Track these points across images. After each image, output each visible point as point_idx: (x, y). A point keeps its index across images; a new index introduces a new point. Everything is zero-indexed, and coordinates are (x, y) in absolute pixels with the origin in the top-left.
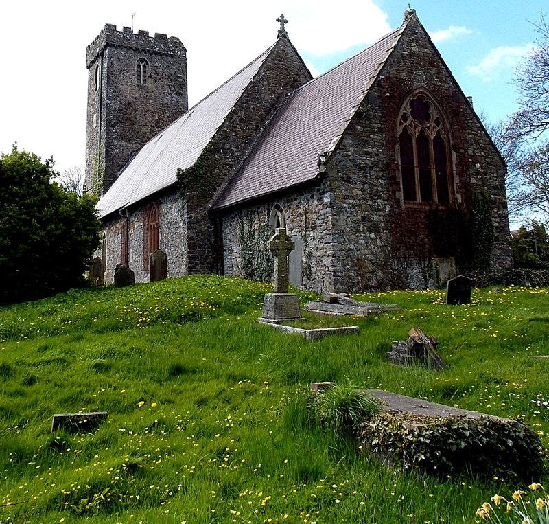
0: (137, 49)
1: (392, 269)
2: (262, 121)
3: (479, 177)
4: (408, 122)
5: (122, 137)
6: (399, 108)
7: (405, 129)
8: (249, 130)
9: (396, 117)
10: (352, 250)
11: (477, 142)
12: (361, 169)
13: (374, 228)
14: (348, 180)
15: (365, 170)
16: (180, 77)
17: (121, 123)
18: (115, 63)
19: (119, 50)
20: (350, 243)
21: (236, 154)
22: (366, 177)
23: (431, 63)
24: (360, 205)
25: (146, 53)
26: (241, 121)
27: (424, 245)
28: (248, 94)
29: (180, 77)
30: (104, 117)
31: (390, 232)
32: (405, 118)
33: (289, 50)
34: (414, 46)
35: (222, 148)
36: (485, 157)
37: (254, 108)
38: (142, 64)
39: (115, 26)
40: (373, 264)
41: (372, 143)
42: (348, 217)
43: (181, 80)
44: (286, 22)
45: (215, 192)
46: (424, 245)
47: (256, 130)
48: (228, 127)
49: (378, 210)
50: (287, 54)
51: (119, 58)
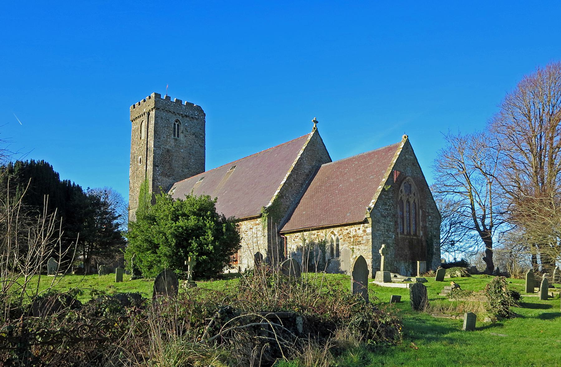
0: (174, 113)
2: (304, 181)
3: (430, 223)
8: (298, 186)
9: (399, 191)
11: (430, 206)
15: (385, 217)
16: (201, 135)
21: (291, 200)
22: (385, 221)
23: (413, 164)
24: (382, 234)
25: (179, 116)
27: (407, 255)
31: (394, 248)
33: (318, 139)
35: (285, 196)
36: (433, 213)
37: (300, 173)
38: (177, 124)
42: (378, 240)
46: (407, 255)
47: (301, 186)
51: (162, 118)
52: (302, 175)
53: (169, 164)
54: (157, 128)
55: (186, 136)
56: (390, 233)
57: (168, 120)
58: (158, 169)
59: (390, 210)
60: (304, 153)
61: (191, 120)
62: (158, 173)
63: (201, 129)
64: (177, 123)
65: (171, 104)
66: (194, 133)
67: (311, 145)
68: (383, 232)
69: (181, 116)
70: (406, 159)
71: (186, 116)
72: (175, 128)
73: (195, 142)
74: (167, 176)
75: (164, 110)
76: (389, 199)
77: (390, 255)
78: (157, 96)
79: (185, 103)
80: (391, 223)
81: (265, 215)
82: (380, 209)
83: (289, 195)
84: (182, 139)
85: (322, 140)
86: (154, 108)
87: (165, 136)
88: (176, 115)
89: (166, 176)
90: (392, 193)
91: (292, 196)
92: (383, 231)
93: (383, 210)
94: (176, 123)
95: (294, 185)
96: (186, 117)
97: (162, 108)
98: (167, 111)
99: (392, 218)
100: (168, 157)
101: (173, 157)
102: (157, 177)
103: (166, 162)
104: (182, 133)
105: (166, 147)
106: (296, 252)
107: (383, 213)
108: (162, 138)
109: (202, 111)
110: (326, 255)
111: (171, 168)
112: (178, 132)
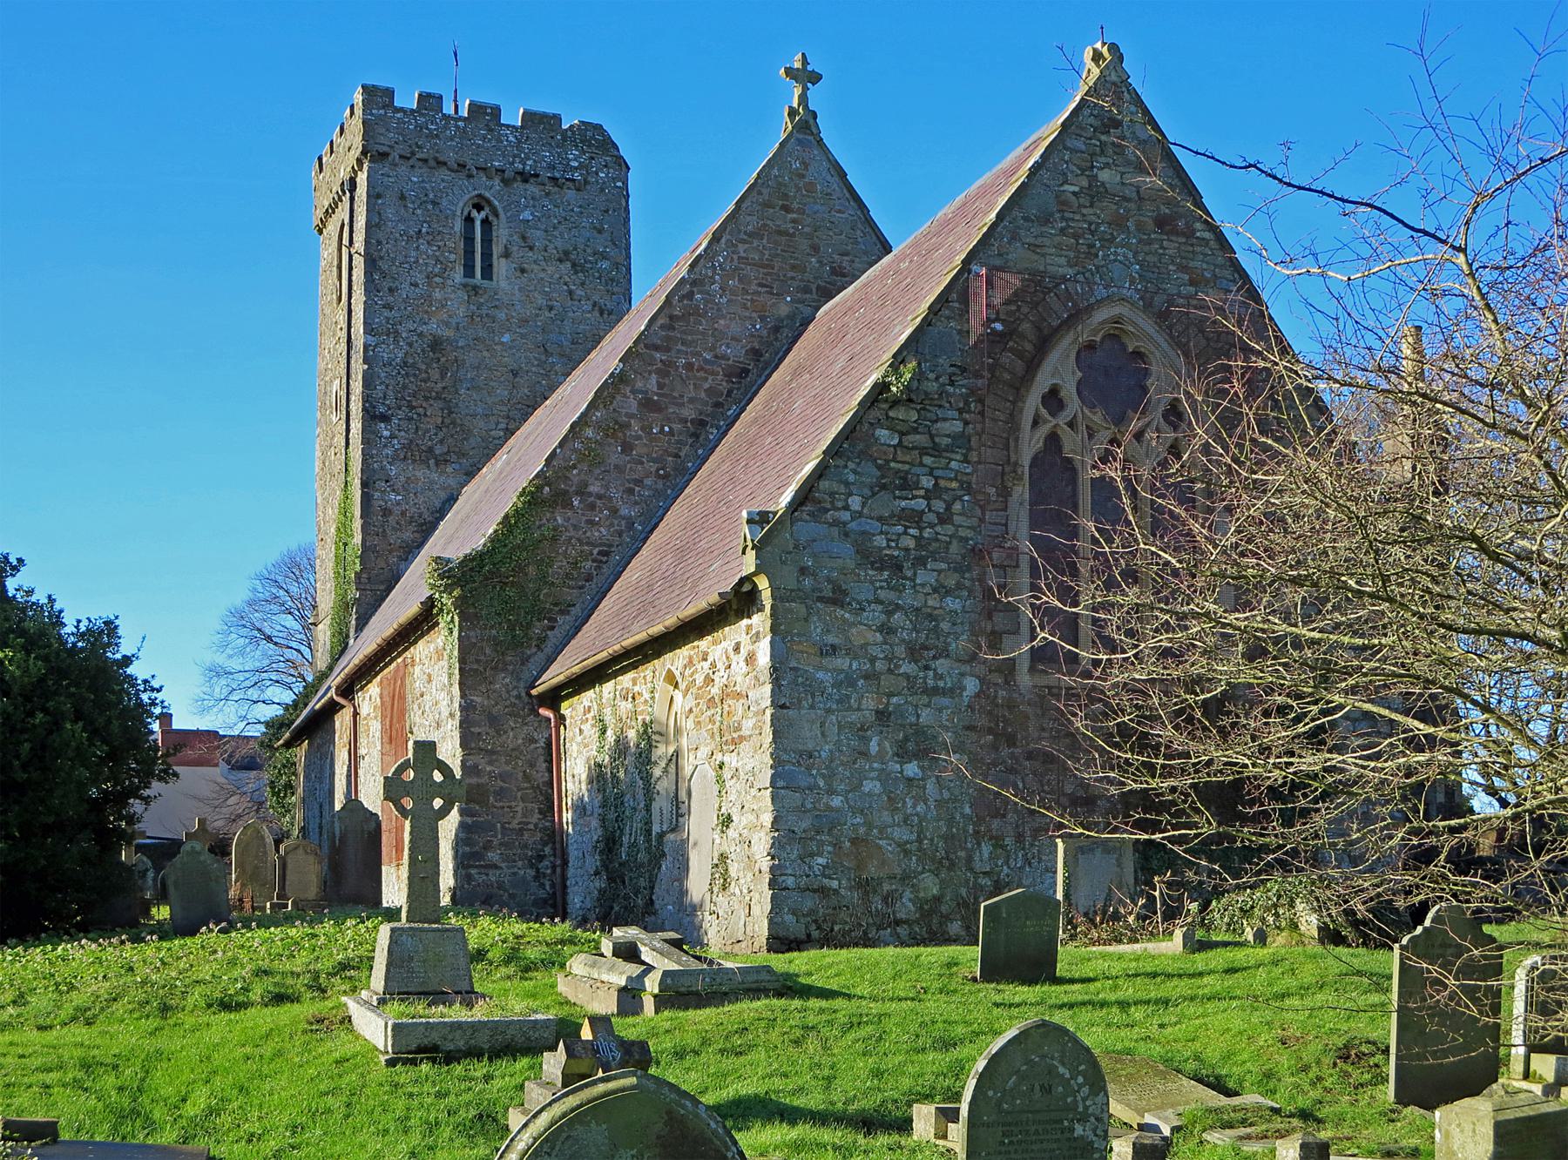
1: (971, 869)
2: (718, 405)
4: (1066, 415)
5: (413, 453)
6: (1033, 365)
7: (1053, 439)
8: (671, 432)
10: (837, 810)
12: (881, 563)
13: (918, 746)
14: (838, 598)
15: (900, 568)
16: (604, 256)
17: (412, 408)
18: (390, 213)
19: (403, 169)
20: (831, 792)
21: (624, 511)
22: (899, 590)
25: (490, 178)
26: (648, 404)
28: (671, 317)
29: (604, 256)
30: (357, 387)
32: (1053, 399)
34: (1107, 165)
35: (580, 493)
37: (689, 366)
38: (478, 217)
39: (390, 93)
40: (907, 853)
41: (927, 482)
42: (829, 711)
43: (605, 265)
44: (815, 78)
45: (552, 628)
47: (696, 436)
48: (598, 426)
49: (936, 691)
50: (810, 187)
51: (403, 197)
52: (702, 374)
53: (440, 404)
54: (379, 243)
55: (523, 271)
56: (942, 665)
57: (434, 203)
58: (386, 433)
59: (944, 519)
60: (716, 254)
61: (548, 194)
62: (389, 452)
63: (600, 232)
64: (483, 214)
65: (446, 127)
66: (566, 253)
67: (767, 205)
68: (873, 660)
69: (497, 181)
70: (1096, 192)
71: (525, 177)
72: (469, 240)
73: (571, 293)
74: (432, 462)
75: (411, 162)
76: (936, 450)
77: (940, 803)
78: (378, 97)
79: (513, 116)
80: (952, 603)
81: (447, 600)
82: (846, 516)
83: (607, 487)
84: (503, 284)
85: (842, 175)
86: (364, 153)
87: (420, 278)
88: (470, 176)
89: (425, 462)
90: (960, 411)
91: (631, 491)
92: (875, 651)
93: (880, 519)
94: (474, 213)
95: (647, 429)
96: (526, 181)
97: (401, 149)
98: (425, 161)
99: (959, 569)
100: (435, 374)
101: (461, 373)
102: (382, 468)
103: (426, 398)
104: (507, 254)
105: (424, 328)
106: (586, 799)
107: (880, 541)
108: (405, 290)
109: (608, 145)
110: (655, 806)
111: (453, 423)
112: (487, 255)
